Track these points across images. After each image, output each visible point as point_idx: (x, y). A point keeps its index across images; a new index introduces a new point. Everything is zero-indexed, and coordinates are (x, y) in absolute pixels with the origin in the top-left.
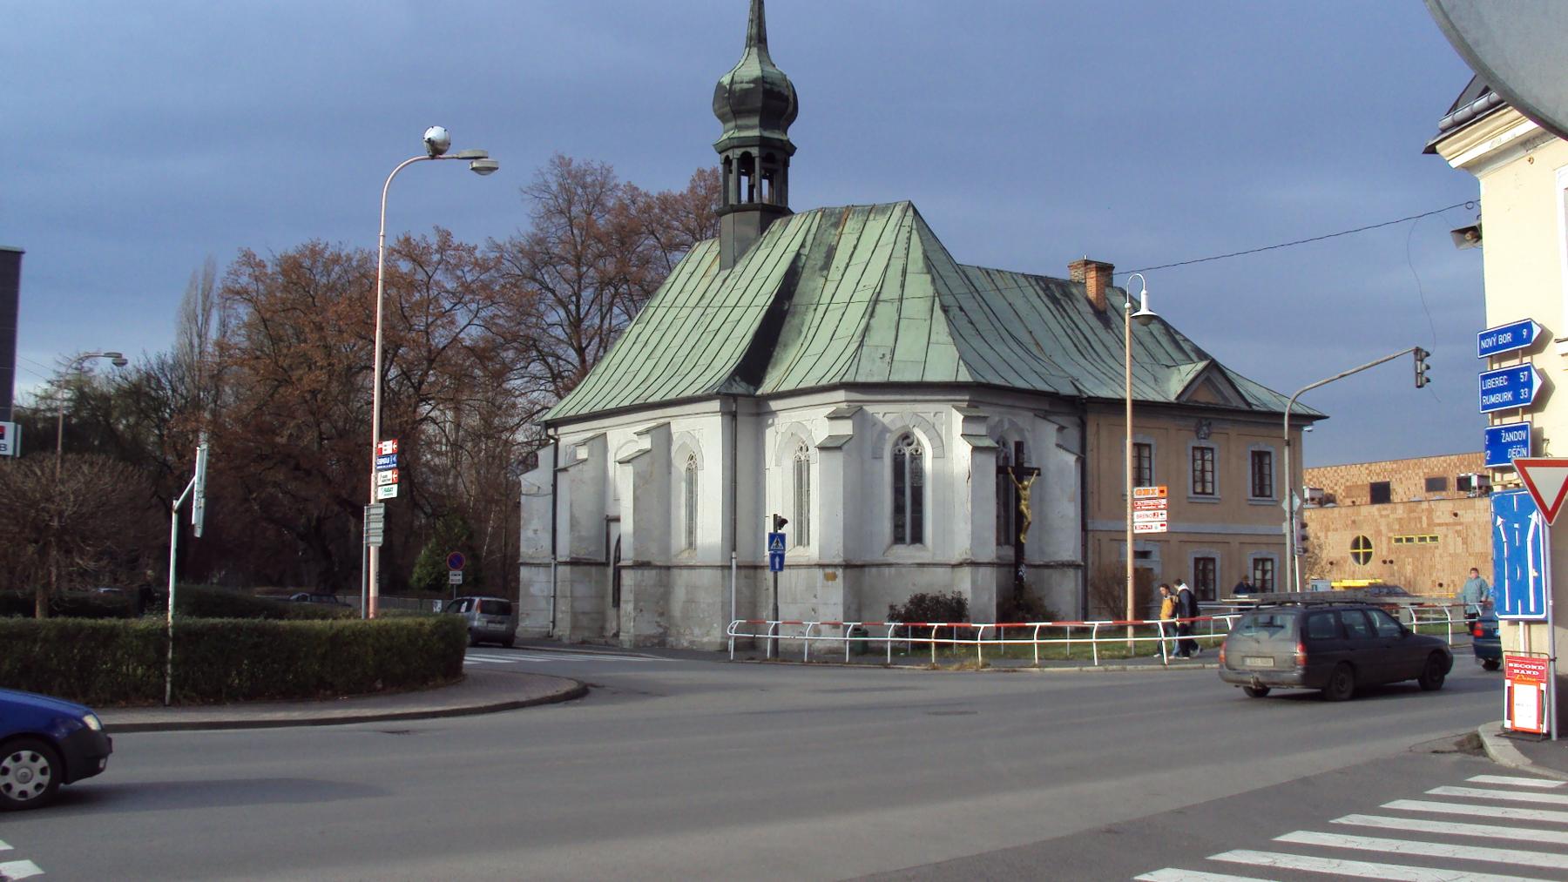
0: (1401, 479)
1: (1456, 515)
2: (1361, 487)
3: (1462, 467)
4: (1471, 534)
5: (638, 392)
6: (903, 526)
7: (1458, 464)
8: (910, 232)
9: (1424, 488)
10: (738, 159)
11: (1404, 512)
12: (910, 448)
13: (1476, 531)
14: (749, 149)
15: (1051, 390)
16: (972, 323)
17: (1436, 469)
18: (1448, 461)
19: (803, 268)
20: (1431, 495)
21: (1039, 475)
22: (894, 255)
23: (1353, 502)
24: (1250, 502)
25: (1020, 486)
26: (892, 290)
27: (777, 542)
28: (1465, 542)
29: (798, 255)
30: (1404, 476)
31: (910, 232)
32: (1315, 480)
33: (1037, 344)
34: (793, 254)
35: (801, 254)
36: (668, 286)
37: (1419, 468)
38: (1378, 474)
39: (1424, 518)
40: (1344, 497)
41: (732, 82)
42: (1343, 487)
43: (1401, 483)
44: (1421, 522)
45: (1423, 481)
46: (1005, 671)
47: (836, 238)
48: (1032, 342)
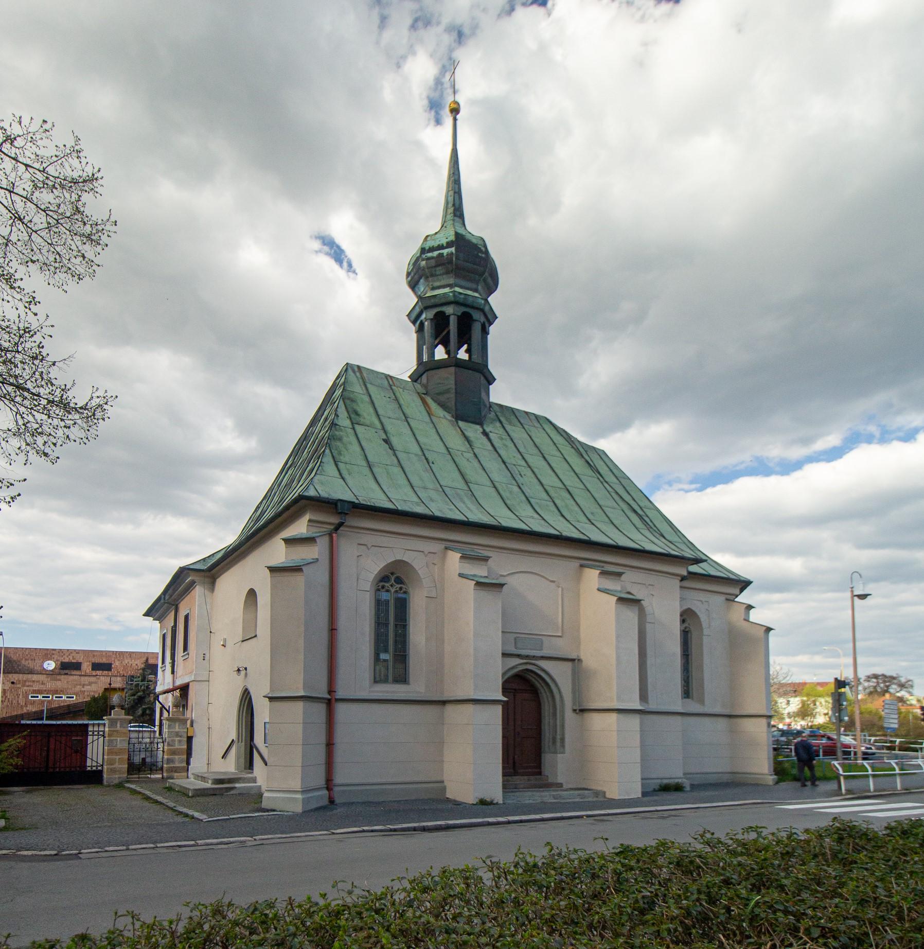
14: (444, 309)
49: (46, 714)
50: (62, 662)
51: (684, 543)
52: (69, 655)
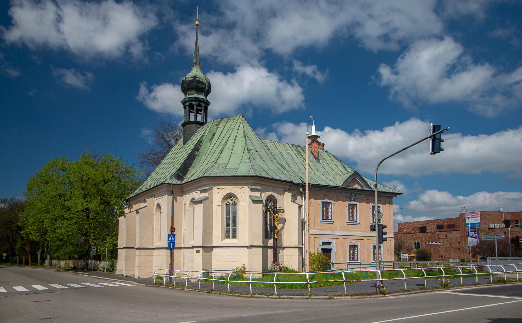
0: (429, 226)
1: (447, 236)
2: (417, 228)
3: (448, 222)
6: (229, 232)
7: (447, 221)
9: (436, 228)
10: (188, 106)
11: (430, 235)
12: (232, 201)
13: (453, 241)
15: (290, 180)
17: (440, 223)
18: (444, 220)
19: (204, 140)
20: (438, 230)
21: (283, 212)
22: (232, 132)
23: (414, 232)
25: (275, 216)
27: (172, 237)
28: (450, 244)
29: (203, 136)
30: (430, 225)
31: (240, 124)
32: (403, 226)
33: (289, 166)
35: (204, 136)
37: (435, 222)
38: (422, 224)
39: (437, 237)
40: (412, 231)
42: (411, 228)
43: (429, 227)
44: (435, 238)
45: (436, 226)
46: (237, 296)
47: (216, 129)
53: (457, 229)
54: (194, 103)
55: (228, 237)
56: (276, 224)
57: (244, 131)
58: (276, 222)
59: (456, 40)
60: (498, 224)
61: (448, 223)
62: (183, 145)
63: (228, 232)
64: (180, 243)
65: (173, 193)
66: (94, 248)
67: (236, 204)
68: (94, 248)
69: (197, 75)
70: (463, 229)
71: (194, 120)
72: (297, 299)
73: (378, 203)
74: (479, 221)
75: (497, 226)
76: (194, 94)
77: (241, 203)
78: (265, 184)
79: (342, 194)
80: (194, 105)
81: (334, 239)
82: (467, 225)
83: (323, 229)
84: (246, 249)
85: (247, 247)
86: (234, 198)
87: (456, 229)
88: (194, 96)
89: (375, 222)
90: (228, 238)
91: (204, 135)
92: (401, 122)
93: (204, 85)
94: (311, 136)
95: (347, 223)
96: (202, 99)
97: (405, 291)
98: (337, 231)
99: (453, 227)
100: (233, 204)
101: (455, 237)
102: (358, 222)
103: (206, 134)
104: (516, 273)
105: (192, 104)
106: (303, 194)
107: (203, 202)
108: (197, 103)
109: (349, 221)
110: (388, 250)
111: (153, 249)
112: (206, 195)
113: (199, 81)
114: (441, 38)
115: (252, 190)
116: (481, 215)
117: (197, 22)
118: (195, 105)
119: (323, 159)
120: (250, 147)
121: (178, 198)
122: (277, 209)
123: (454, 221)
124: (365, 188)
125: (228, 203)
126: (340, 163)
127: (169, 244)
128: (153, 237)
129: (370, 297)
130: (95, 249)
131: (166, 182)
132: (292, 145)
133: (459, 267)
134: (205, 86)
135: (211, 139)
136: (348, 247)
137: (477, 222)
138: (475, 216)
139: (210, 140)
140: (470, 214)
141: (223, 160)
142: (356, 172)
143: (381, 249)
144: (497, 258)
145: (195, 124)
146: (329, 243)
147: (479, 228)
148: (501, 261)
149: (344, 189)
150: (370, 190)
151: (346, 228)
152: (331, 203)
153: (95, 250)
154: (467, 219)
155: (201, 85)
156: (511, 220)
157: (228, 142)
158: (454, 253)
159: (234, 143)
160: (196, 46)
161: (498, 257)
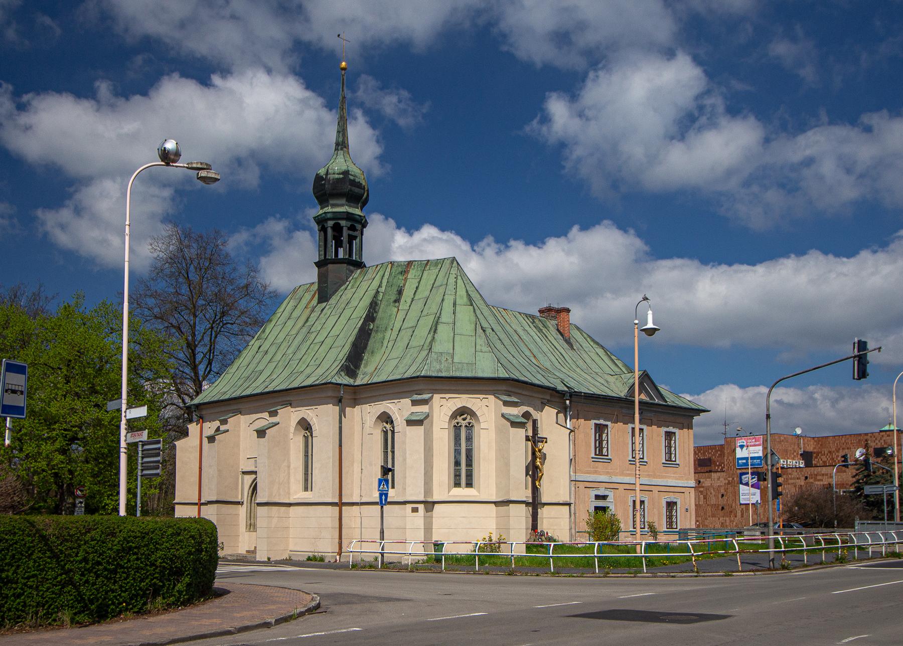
1: (700, 482)
3: (699, 454)
4: (709, 493)
5: (267, 384)
6: (460, 476)
7: (697, 452)
8: (456, 278)
13: (712, 491)
14: (339, 221)
16: (500, 340)
19: (381, 301)
21: (546, 442)
24: (664, 465)
26: (446, 317)
27: (384, 484)
28: (705, 498)
29: (378, 292)
31: (456, 278)
33: (535, 357)
34: (374, 292)
35: (379, 292)
36: (279, 315)
41: (327, 173)
48: (532, 355)
49: (749, 507)
50: (874, 449)
51: (487, 306)
52: (881, 439)
53: (717, 468)
54: (343, 223)
55: (457, 484)
56: (538, 463)
57: (467, 291)
58: (538, 459)
59: (697, 60)
60: (793, 459)
61: (699, 456)
62: (320, 301)
63: (457, 476)
64: (352, 495)
65: (340, 401)
66: (81, 503)
67: (472, 426)
68: (81, 503)
69: (350, 169)
70: (731, 470)
71: (342, 257)
72: (681, 577)
73: (641, 422)
74: (760, 454)
75: (791, 463)
76: (342, 205)
77: (483, 425)
78: (520, 391)
79: (623, 411)
80: (344, 228)
81: (612, 490)
82: (738, 462)
83: (596, 472)
84: (493, 506)
85: (495, 503)
86: (469, 416)
87: (713, 469)
88: (345, 210)
89: (634, 458)
90: (459, 487)
91: (379, 290)
92: (585, 228)
93: (361, 188)
94: (645, 329)
95: (630, 462)
96: (358, 217)
97: (806, 566)
98: (616, 476)
99: (709, 464)
100: (466, 426)
101: (717, 484)
102: (677, 462)
103: (383, 288)
104: (882, 547)
105: (339, 224)
106: (568, 410)
107: (424, 422)
108: (349, 224)
109: (666, 461)
110: (687, 510)
111: (290, 505)
112: (424, 409)
113: (354, 181)
114: (669, 54)
115: (506, 404)
116: (765, 441)
117: (344, 64)
118: (346, 226)
119: (577, 344)
120: (485, 325)
121: (348, 409)
122: (538, 437)
123: (710, 451)
124: (657, 400)
125: (458, 424)
126: (603, 351)
127: (381, 495)
128: (289, 483)
129: (776, 573)
130: (83, 505)
131: (334, 381)
132: (526, 315)
133: (853, 534)
134: (362, 191)
135: (397, 301)
136: (664, 505)
137: (756, 455)
138: (753, 444)
139: (395, 301)
140: (745, 439)
141: (442, 344)
142: (645, 371)
143: (676, 508)
144: (886, 522)
145: (346, 265)
146: (604, 497)
147: (760, 468)
148: (870, 526)
149: (628, 401)
150: (664, 403)
151: (628, 470)
152: (607, 426)
153: (82, 507)
154: (738, 450)
155: (356, 190)
156: (815, 453)
157: (443, 310)
158: (713, 516)
159: (454, 313)
160: (343, 110)
161: (888, 520)
